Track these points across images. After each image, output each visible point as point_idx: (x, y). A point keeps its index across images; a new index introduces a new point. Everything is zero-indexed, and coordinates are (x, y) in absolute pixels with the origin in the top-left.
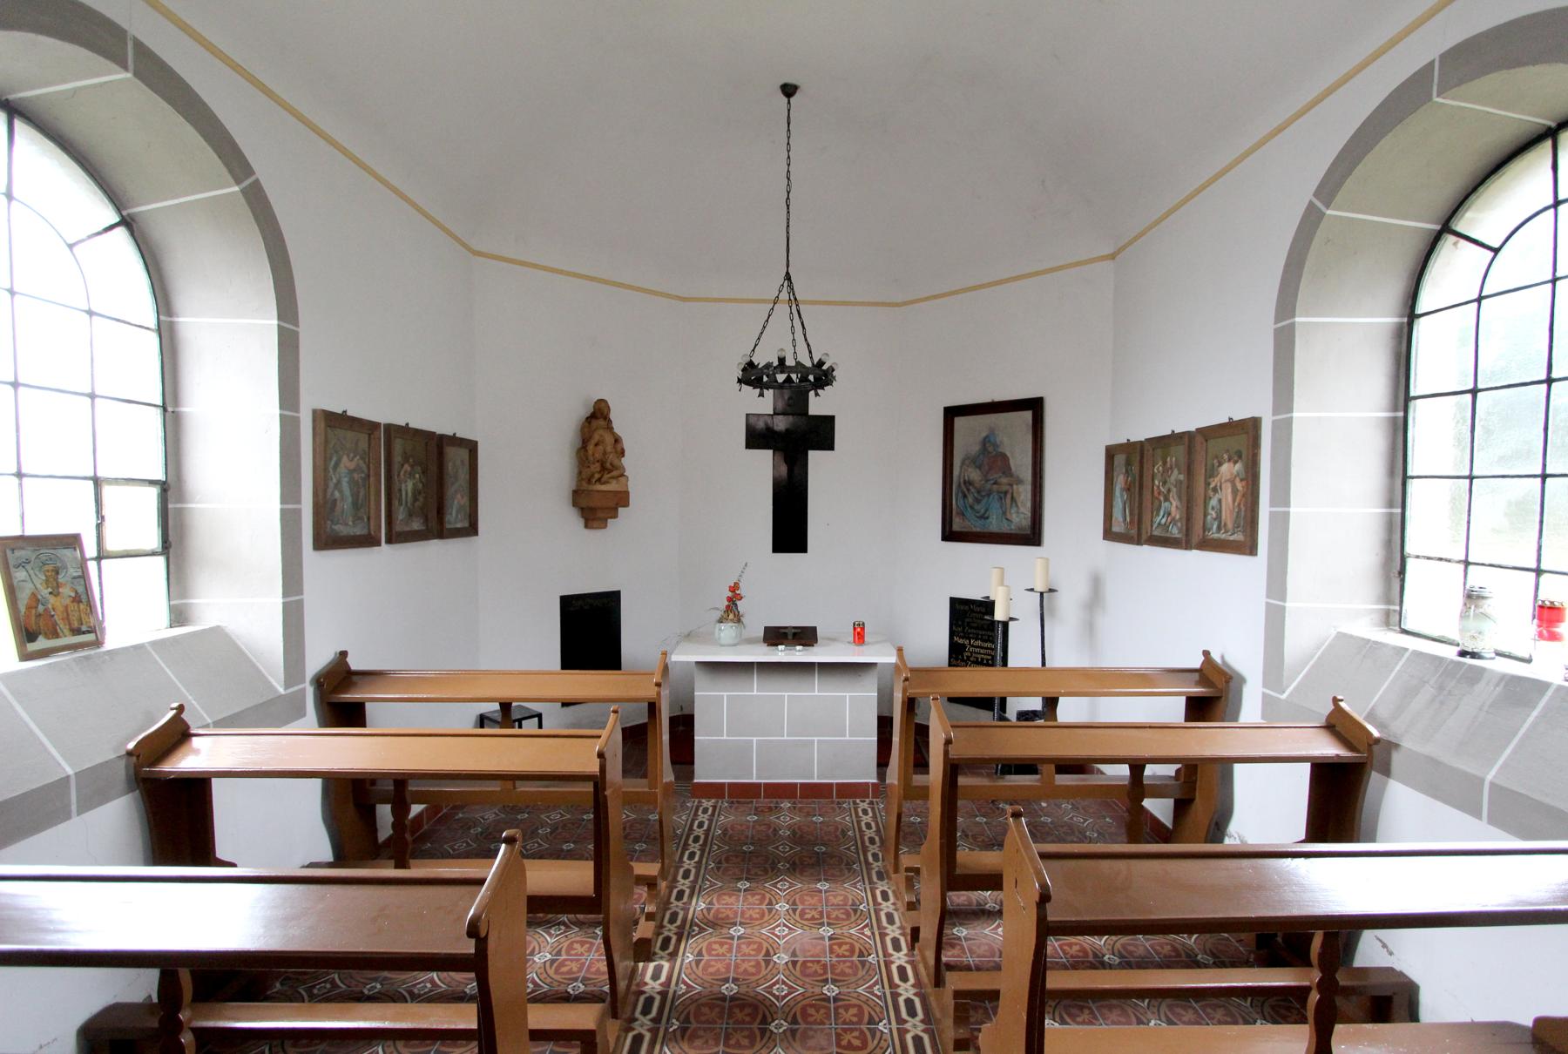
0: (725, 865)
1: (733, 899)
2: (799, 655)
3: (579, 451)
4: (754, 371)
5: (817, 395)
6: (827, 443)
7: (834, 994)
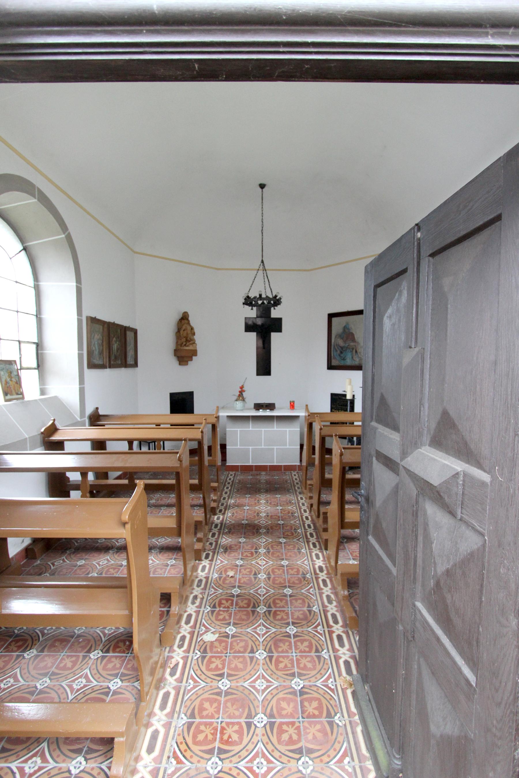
0: (240, 490)
1: (244, 499)
2: (268, 413)
3: (177, 333)
4: (249, 300)
5: (274, 309)
6: (279, 329)
7: (290, 627)
